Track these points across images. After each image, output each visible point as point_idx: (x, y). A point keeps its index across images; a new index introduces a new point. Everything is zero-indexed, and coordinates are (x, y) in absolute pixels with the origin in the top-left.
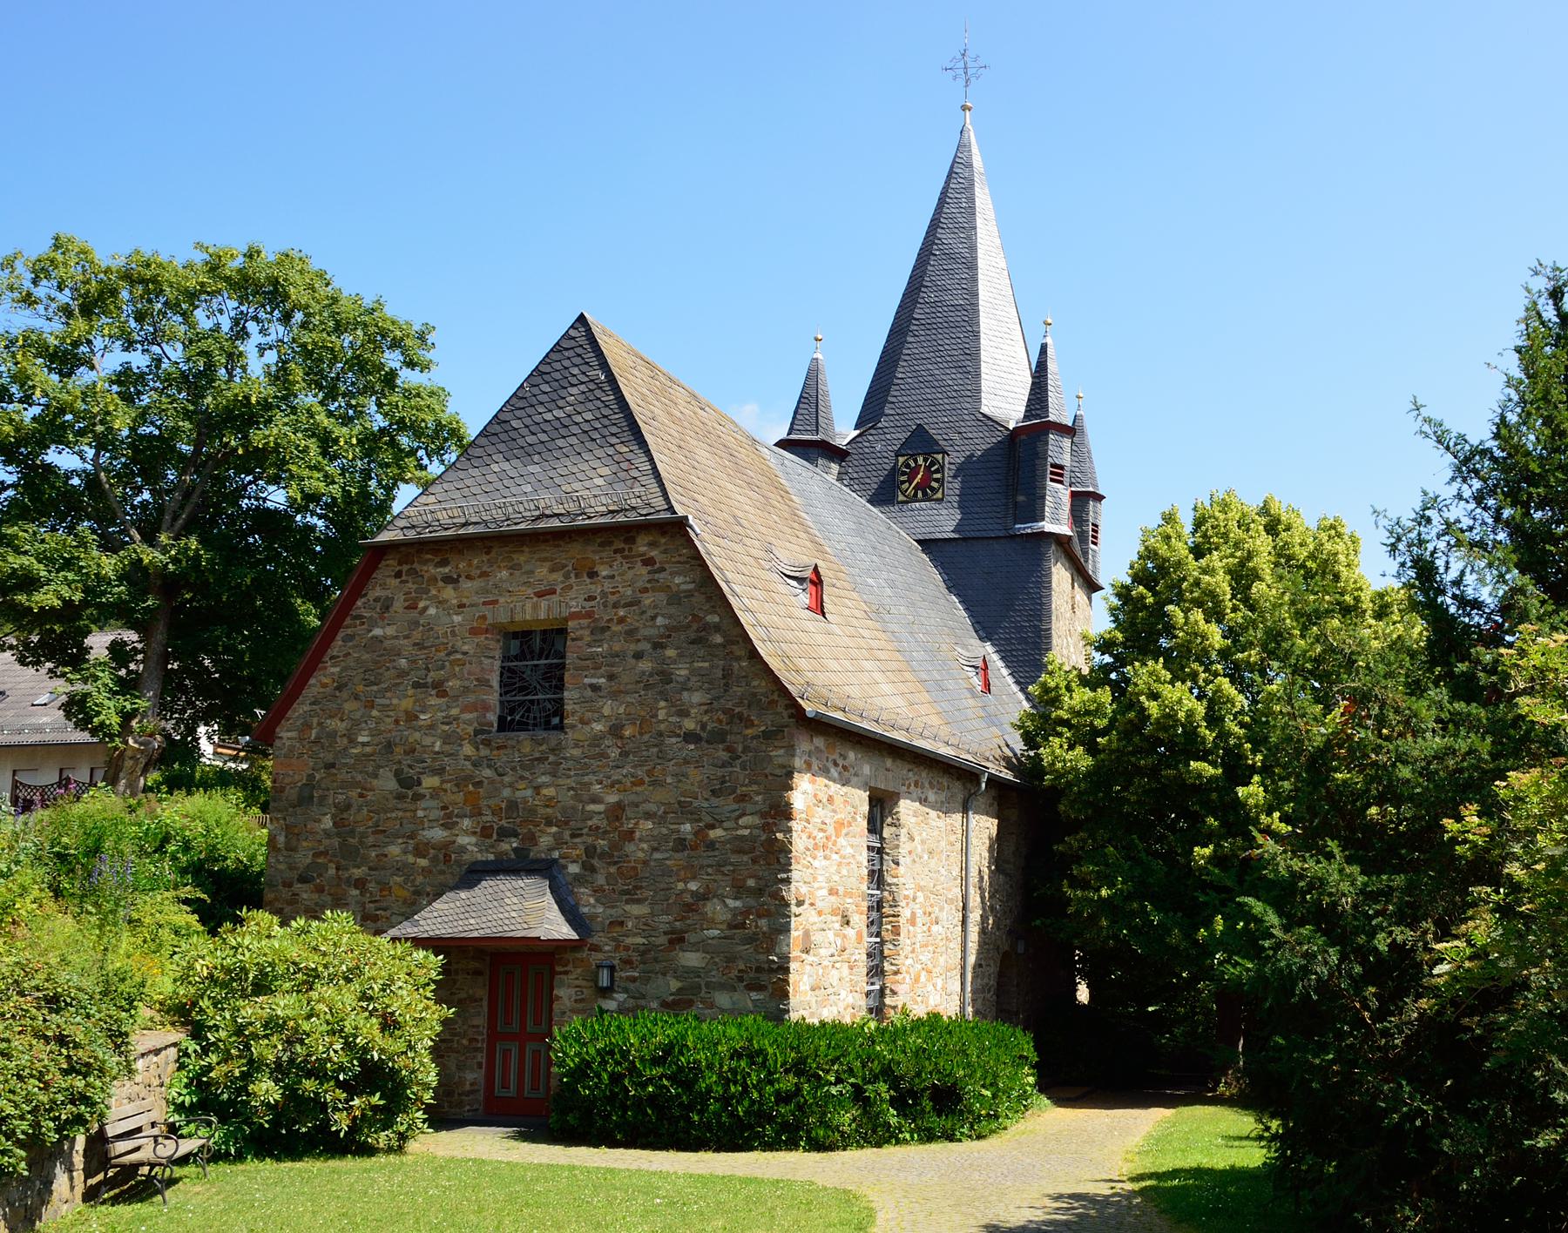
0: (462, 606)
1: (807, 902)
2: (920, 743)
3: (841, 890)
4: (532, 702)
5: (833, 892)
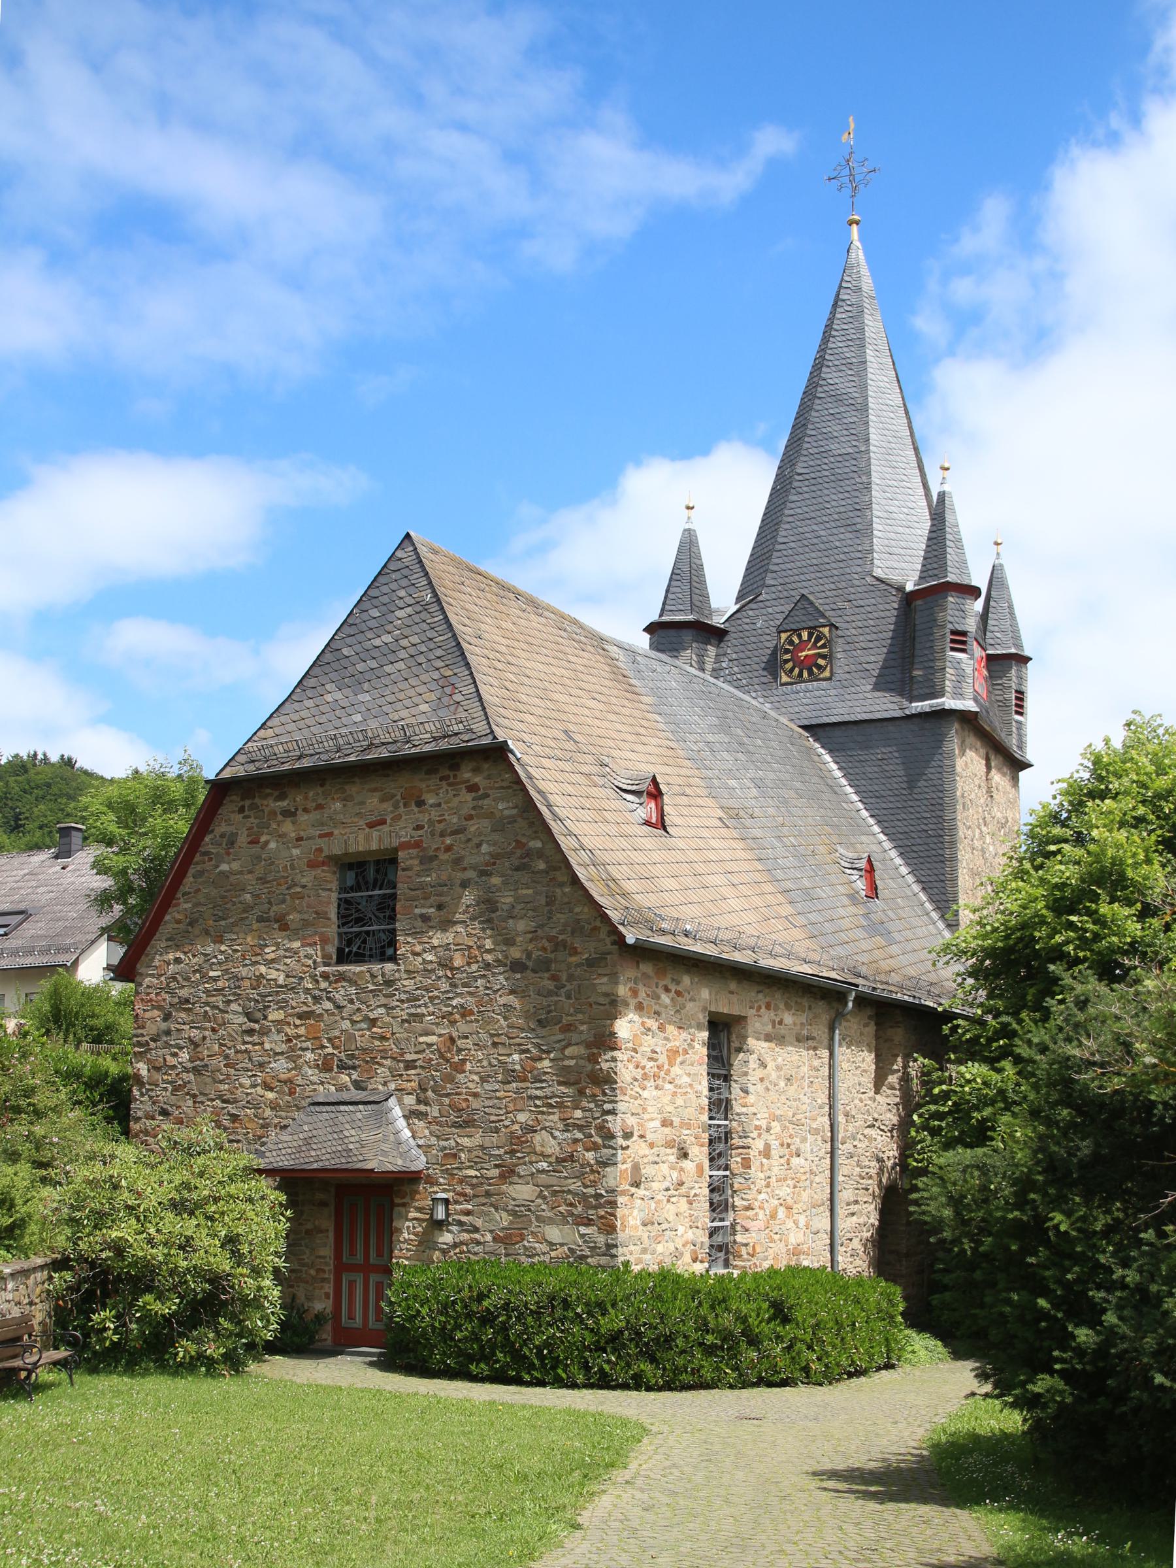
0: (299, 839)
1: (636, 1134)
2: (766, 962)
3: (676, 1121)
4: (367, 933)
5: (666, 1123)
